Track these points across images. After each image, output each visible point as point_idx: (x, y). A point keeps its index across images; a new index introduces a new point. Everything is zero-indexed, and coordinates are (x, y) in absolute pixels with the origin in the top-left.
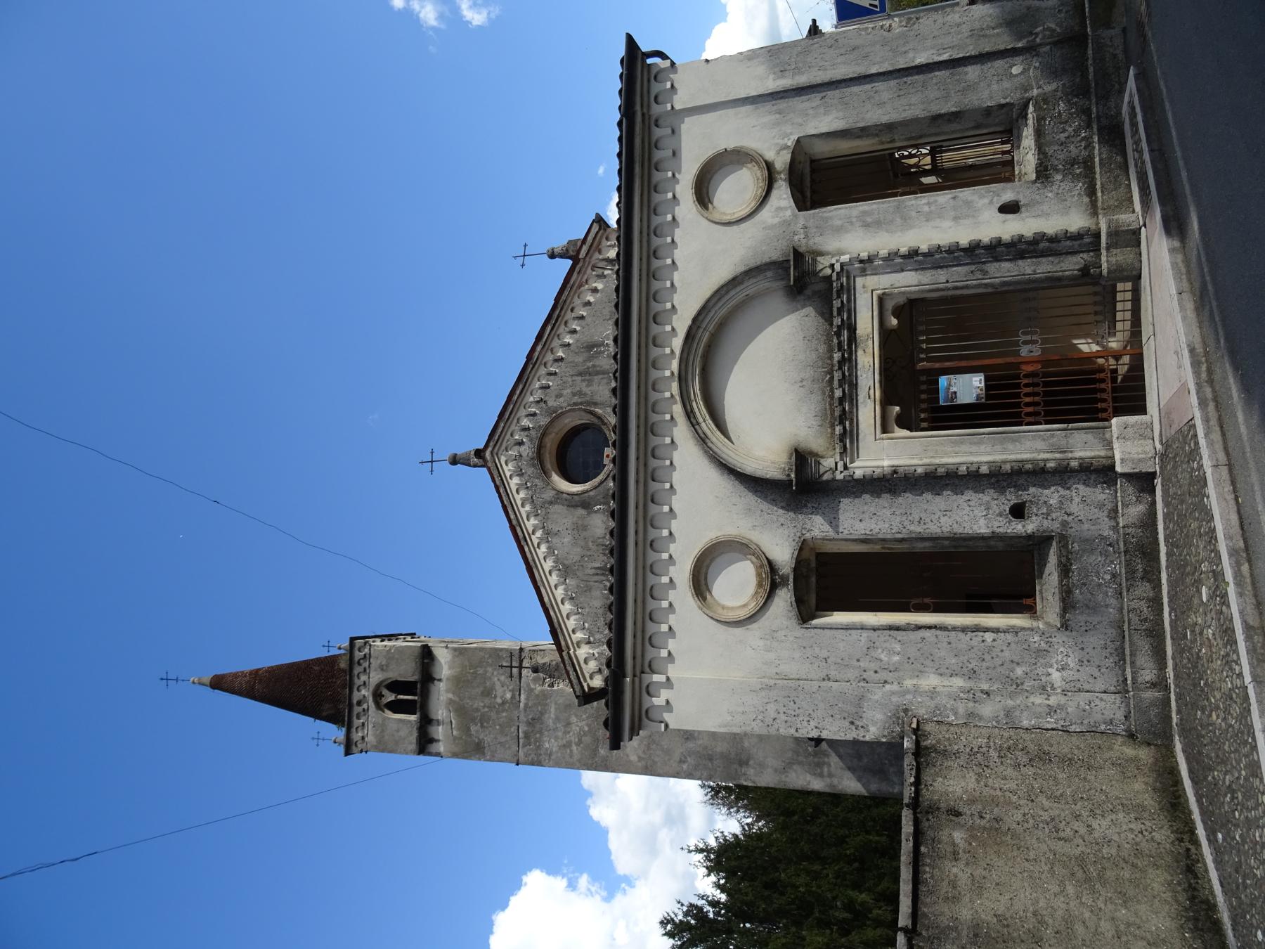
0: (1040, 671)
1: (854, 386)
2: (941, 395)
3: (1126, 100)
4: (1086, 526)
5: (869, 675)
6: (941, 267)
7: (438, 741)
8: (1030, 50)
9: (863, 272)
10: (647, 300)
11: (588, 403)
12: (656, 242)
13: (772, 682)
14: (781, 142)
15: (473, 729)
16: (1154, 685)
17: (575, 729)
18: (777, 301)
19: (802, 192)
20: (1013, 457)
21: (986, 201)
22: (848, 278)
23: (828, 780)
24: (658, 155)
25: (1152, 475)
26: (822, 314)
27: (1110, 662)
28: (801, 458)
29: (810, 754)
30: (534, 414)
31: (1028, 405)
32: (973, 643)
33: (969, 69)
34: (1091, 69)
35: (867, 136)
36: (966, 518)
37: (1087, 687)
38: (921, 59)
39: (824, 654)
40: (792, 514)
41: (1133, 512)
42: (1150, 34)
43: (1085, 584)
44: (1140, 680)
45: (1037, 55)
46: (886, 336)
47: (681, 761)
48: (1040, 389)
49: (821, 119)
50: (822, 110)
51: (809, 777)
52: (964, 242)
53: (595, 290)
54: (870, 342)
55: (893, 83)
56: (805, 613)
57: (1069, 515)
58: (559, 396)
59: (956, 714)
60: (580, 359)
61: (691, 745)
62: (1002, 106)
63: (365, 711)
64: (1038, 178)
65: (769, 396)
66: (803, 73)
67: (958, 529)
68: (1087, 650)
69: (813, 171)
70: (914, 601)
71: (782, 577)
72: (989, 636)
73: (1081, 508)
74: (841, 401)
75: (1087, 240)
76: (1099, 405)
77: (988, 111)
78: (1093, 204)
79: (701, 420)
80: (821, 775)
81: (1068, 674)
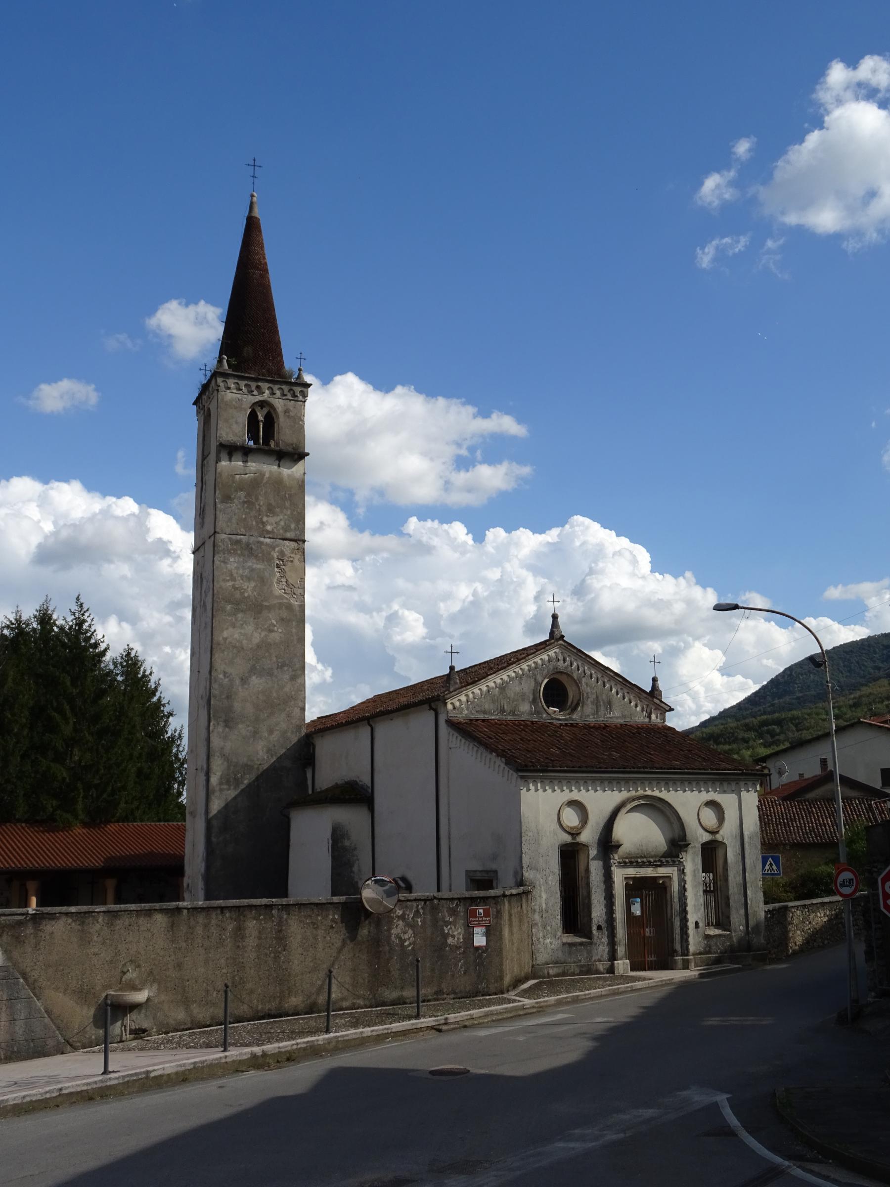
1: (641, 867)
7: (230, 460)
8: (747, 932)
9: (679, 870)
11: (583, 702)
12: (694, 784)
15: (242, 494)
17: (245, 585)
23: (217, 788)
24: (725, 784)
25: (613, 973)
26: (665, 853)
29: (236, 775)
38: (749, 892)
41: (601, 967)
46: (655, 879)
47: (225, 673)
49: (732, 854)
51: (219, 774)
52: (688, 908)
53: (636, 706)
58: (587, 684)
60: (604, 697)
61: (238, 681)
63: (251, 392)
65: (638, 831)
73: (602, 949)
74: (637, 862)
78: (697, 954)
80: (221, 783)
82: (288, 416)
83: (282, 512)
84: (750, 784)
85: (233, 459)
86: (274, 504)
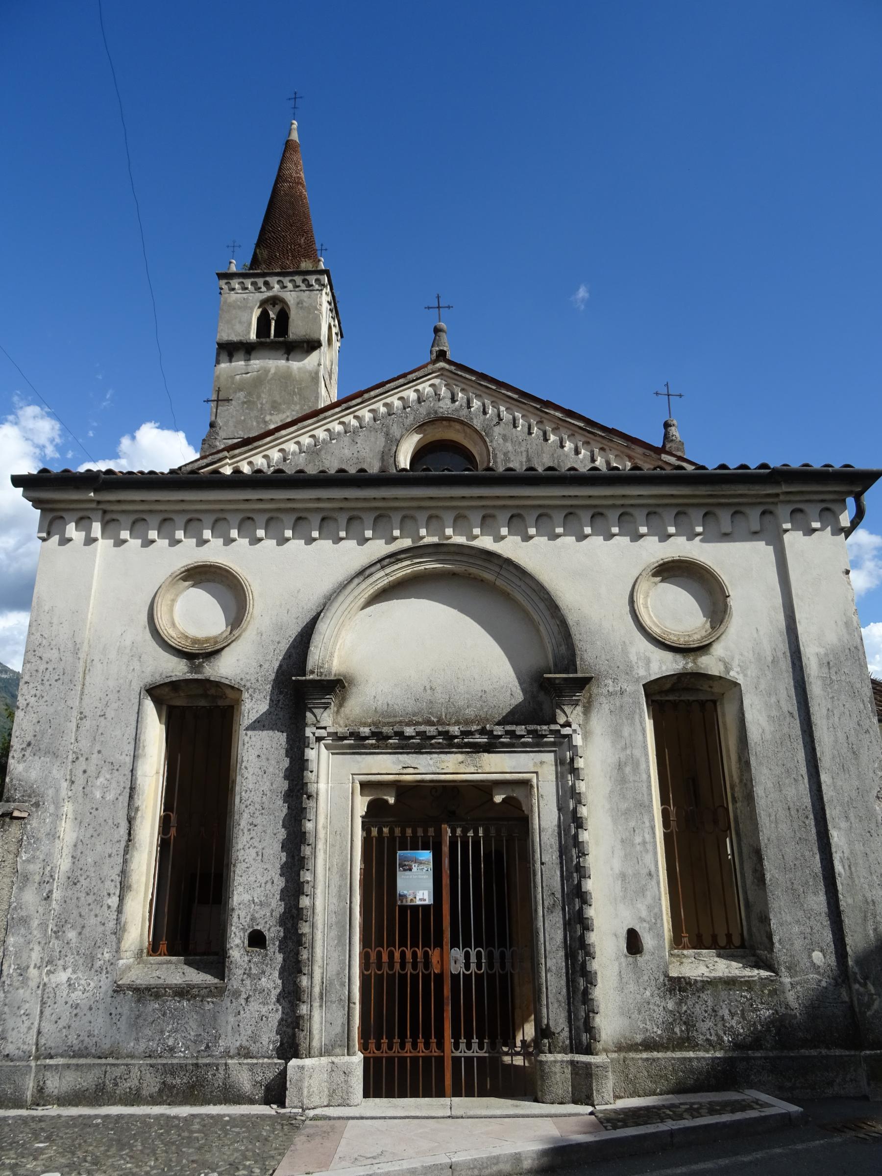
0: (70, 959)
1: (418, 750)
2: (409, 853)
3: (764, 1097)
4: (232, 1019)
5: (82, 764)
6: (561, 857)
8: (842, 972)
10: (540, 506)
13: (82, 655)
14: (735, 664)
15: (241, 395)
16: (41, 1090)
18: (533, 660)
19: (672, 690)
20: (319, 936)
21: (644, 914)
22: (553, 744)
26: (512, 713)
27: (73, 1039)
28: (335, 687)
30: (485, 413)
31: (391, 955)
32: (108, 883)
33: (822, 898)
34: (814, 1052)
35: (741, 771)
36: (253, 879)
37: (47, 1012)
38: (837, 837)
39: (110, 713)
40: (273, 676)
41: (244, 1078)
42: (838, 1139)
43: (164, 1015)
44: (48, 1074)
45: (837, 984)
46: (485, 788)
48: (409, 969)
49: (762, 714)
50: (774, 713)
52: (589, 885)
54: (473, 770)
55: (807, 801)
56: (161, 693)
57: (247, 999)
58: (505, 438)
59: (28, 861)
62: (770, 937)
63: (258, 289)
64: (671, 979)
65: (416, 652)
66: (824, 689)
67: (239, 869)
68: (88, 1014)
69: (702, 704)
70: (173, 816)
71: (200, 666)
72: (114, 901)
73: (251, 1013)
74: (400, 735)
75: (585, 1037)
76: (385, 1040)
77: (765, 920)
78: (633, 1047)
79: (388, 570)
81: (64, 991)
82: (301, 308)
83: (289, 408)
84: (813, 510)
85: (233, 359)
86: (279, 401)
